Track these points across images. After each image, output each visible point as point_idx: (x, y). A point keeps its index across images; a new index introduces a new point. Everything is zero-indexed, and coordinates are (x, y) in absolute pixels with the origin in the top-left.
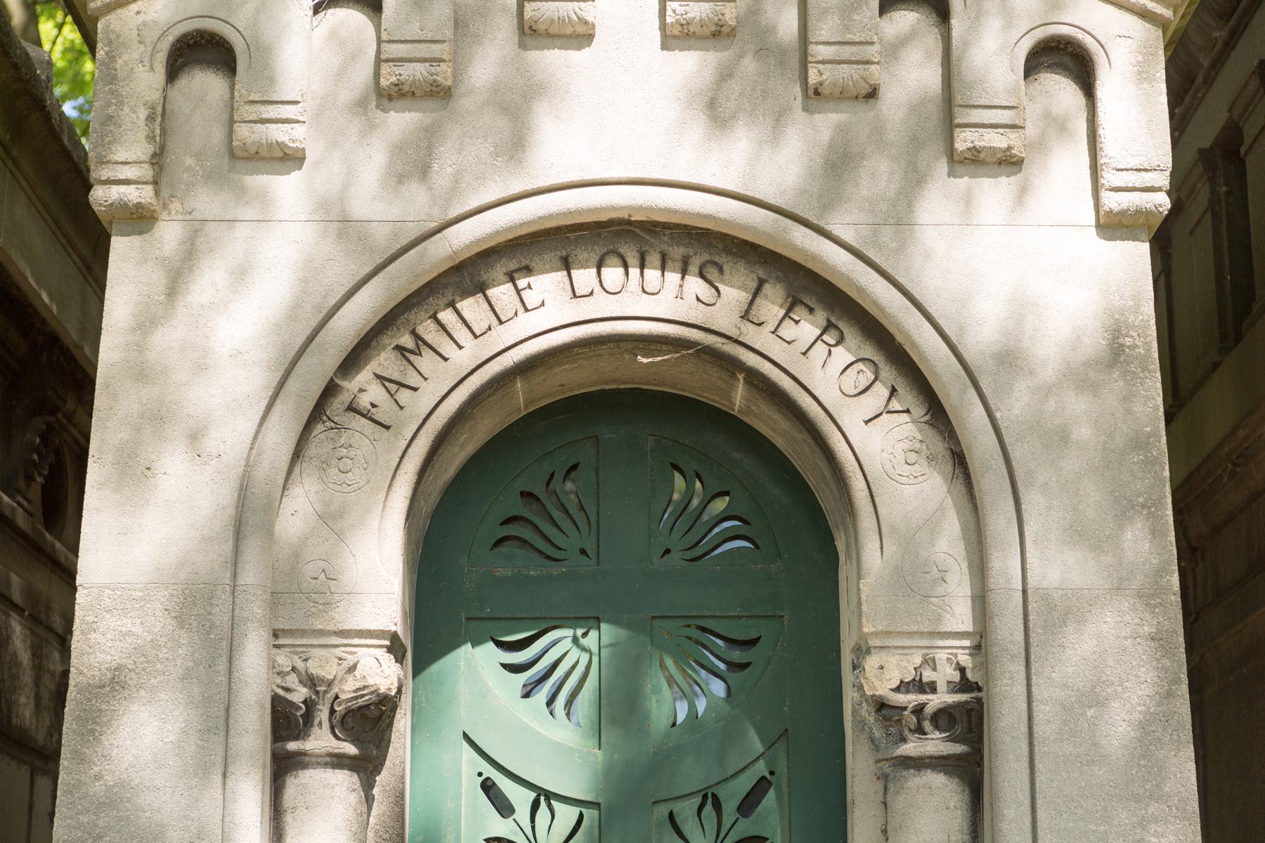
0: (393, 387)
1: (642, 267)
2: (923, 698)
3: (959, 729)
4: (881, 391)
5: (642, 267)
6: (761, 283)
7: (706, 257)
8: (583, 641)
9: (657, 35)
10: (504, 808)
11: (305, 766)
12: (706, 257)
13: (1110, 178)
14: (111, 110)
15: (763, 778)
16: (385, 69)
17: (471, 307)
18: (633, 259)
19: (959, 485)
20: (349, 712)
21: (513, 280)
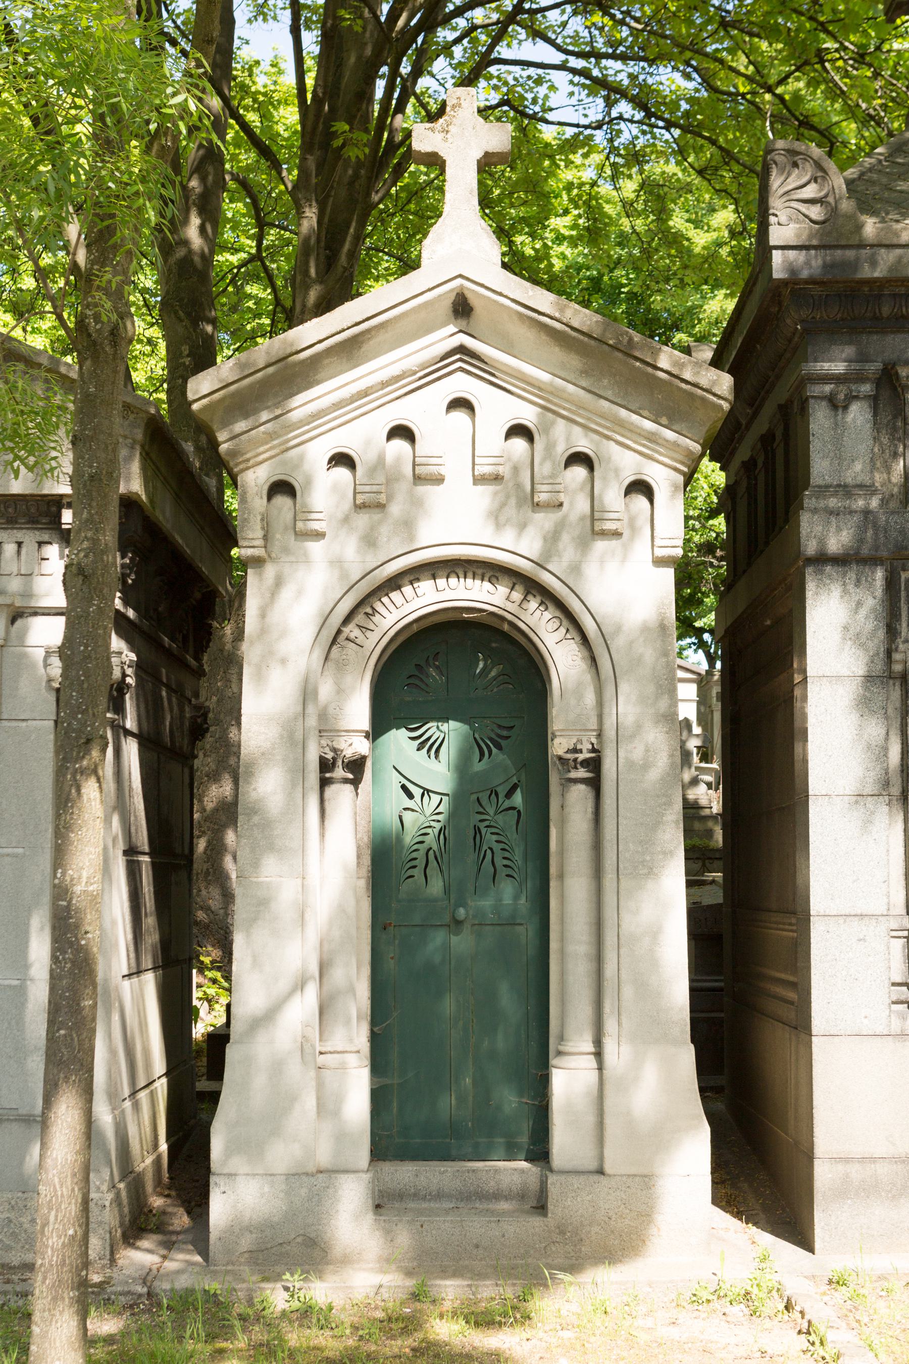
0: (364, 630)
1: (465, 578)
2: (577, 755)
3: (591, 767)
4: (563, 630)
5: (465, 578)
6: (514, 584)
7: (491, 573)
8: (441, 728)
9: (471, 478)
10: (410, 796)
11: (332, 783)
12: (491, 573)
13: (658, 542)
14: (246, 516)
15: (515, 784)
16: (358, 496)
17: (395, 595)
18: (461, 575)
19: (594, 670)
20: (350, 762)
21: (412, 584)
